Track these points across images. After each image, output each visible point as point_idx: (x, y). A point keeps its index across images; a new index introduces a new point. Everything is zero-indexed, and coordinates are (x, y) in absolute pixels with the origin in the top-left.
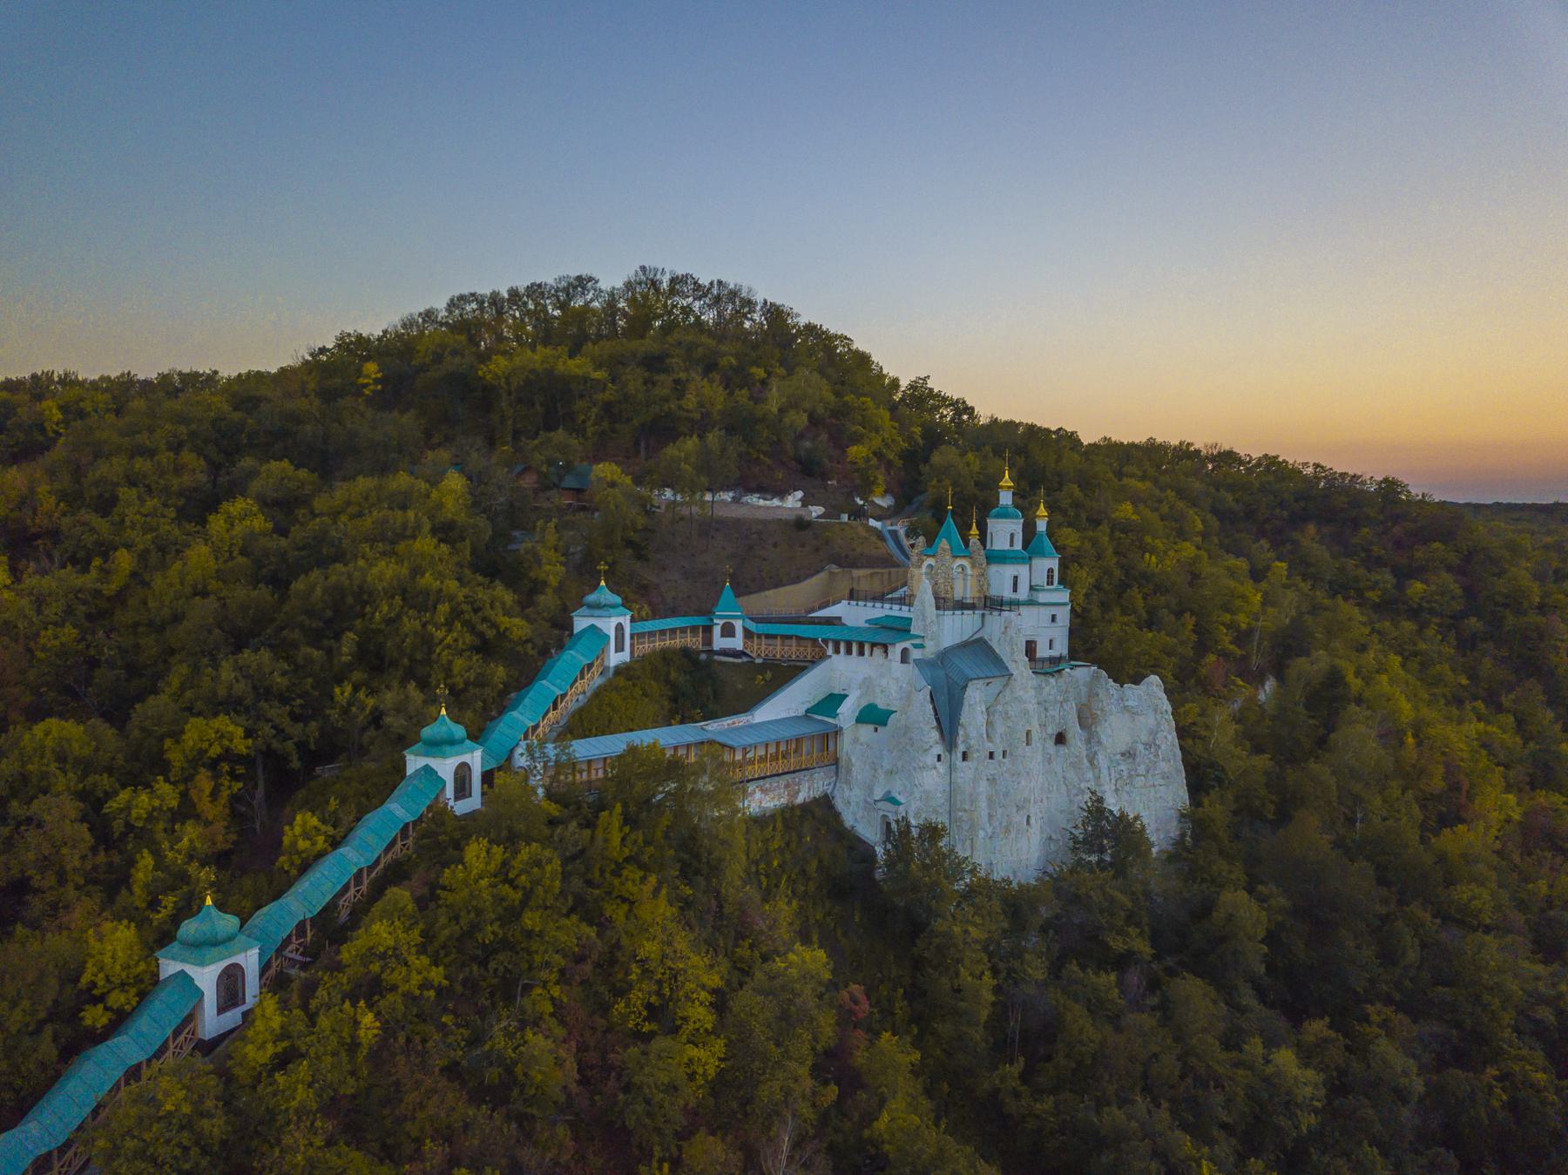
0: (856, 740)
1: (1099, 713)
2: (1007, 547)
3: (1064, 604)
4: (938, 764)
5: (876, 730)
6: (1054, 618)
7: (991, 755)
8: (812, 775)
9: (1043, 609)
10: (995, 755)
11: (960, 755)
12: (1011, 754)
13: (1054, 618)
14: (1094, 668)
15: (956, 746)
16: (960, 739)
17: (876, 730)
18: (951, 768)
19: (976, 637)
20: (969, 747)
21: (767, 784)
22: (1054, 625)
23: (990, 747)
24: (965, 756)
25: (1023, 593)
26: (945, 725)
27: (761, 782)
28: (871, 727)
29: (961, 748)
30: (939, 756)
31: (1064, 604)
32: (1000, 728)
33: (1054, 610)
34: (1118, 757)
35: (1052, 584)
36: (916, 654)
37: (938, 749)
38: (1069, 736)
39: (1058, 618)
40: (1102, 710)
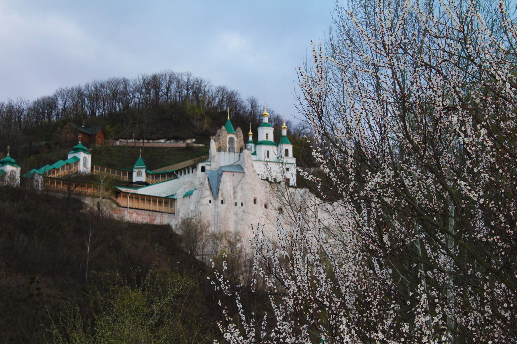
0: (183, 204)
7: (236, 204)
8: (162, 215)
10: (238, 204)
11: (220, 202)
12: (245, 204)
14: (304, 189)
15: (218, 197)
16: (220, 195)
18: (216, 206)
19: (237, 163)
20: (224, 199)
21: (139, 212)
23: (236, 201)
24: (222, 202)
26: (214, 189)
27: (136, 210)
28: (188, 197)
29: (220, 198)
30: (210, 202)
32: (239, 194)
36: (207, 168)
37: (211, 198)
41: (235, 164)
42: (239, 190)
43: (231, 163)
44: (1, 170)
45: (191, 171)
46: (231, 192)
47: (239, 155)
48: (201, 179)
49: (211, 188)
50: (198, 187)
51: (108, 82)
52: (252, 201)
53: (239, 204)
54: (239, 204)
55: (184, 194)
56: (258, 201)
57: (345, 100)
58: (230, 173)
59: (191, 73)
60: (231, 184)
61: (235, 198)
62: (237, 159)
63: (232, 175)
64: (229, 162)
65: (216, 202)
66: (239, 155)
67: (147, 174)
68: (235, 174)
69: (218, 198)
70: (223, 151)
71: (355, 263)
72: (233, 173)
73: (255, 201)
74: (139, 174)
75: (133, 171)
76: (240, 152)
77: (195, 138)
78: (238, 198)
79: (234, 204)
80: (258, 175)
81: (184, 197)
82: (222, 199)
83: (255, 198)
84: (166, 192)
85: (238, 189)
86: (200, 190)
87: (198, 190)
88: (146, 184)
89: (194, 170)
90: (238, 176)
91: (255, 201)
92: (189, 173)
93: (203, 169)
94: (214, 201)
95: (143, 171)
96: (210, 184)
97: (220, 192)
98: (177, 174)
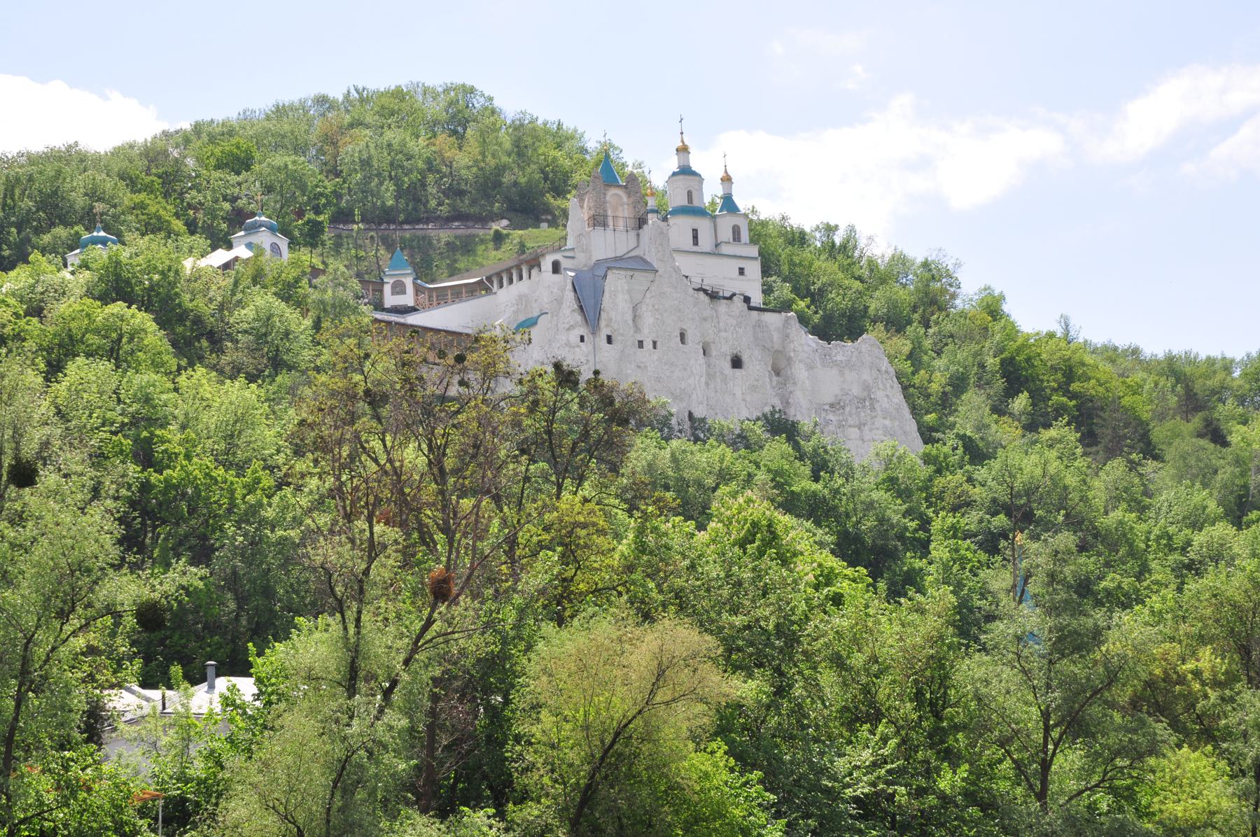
1: (792, 354)
2: (685, 203)
3: (755, 259)
6: (741, 271)
7: (641, 344)
9: (725, 260)
13: (741, 271)
16: (603, 323)
22: (742, 277)
24: (609, 340)
25: (706, 242)
29: (604, 332)
30: (582, 339)
31: (755, 259)
33: (742, 264)
36: (565, 263)
37: (582, 331)
39: (746, 272)
40: (794, 351)
41: (629, 255)
42: (645, 310)
43: (619, 254)
45: (525, 275)
46: (629, 317)
47: (638, 235)
48: (555, 291)
49: (581, 307)
51: (112, 153)
53: (648, 345)
54: (648, 345)
56: (689, 336)
57: (426, 646)
58: (623, 273)
60: (627, 297)
61: (637, 329)
62: (632, 244)
63: (629, 278)
65: (597, 339)
66: (638, 235)
67: (418, 290)
68: (637, 274)
72: (631, 273)
73: (682, 337)
74: (399, 289)
75: (382, 283)
76: (640, 228)
78: (646, 331)
83: (682, 329)
84: (470, 325)
86: (552, 317)
87: (549, 315)
88: (413, 310)
89: (534, 272)
90: (642, 279)
92: (521, 278)
93: (556, 268)
95: (408, 282)
97: (603, 315)
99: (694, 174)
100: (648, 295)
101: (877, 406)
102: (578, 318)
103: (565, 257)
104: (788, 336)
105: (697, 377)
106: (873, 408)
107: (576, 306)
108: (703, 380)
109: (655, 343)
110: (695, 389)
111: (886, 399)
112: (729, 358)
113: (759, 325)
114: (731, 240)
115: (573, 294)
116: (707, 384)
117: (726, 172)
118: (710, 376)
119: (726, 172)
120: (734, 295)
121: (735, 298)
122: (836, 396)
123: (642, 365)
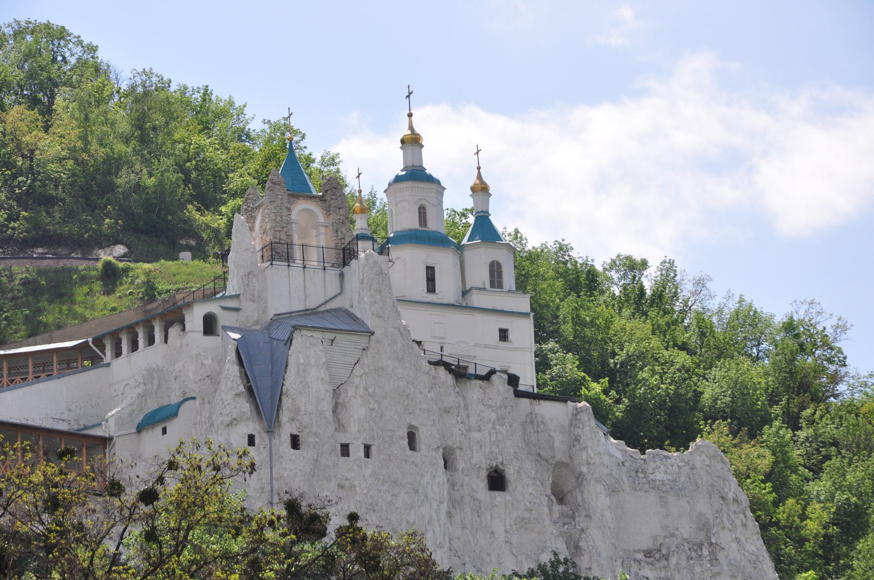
1: (584, 469)
3: (525, 315)
4: (250, 449)
5: (164, 431)
6: (504, 335)
7: (345, 450)
9: (479, 317)
10: (352, 449)
13: (504, 335)
16: (285, 416)
17: (164, 431)
22: (504, 344)
24: (295, 442)
28: (159, 430)
29: (287, 429)
30: (251, 440)
31: (525, 315)
34: (640, 556)
35: (500, 286)
36: (224, 319)
37: (253, 427)
38: (510, 473)
39: (511, 335)
41: (322, 309)
43: (312, 305)
44: (2, 549)
45: (158, 335)
46: (327, 406)
47: (342, 275)
49: (250, 390)
50: (193, 389)
52: (402, 438)
53: (356, 451)
54: (356, 451)
55: (140, 419)
56: (422, 437)
58: (318, 335)
59: (97, 46)
61: (340, 426)
63: (327, 343)
64: (306, 297)
66: (342, 275)
68: (340, 337)
69: (280, 426)
70: (280, 260)
71: (295, 561)
73: (412, 439)
76: (345, 263)
77: (121, 243)
78: (353, 428)
79: (339, 447)
80: (416, 346)
81: (140, 429)
82: (295, 432)
84: (65, 417)
85: (351, 393)
86: (202, 404)
87: (198, 401)
89: (174, 331)
91: (412, 439)
92: (151, 341)
94: (265, 435)
96: (245, 377)
97: (286, 403)
98: (102, 348)
99: (430, 179)
100: (358, 371)
101: (721, 555)
102: (245, 406)
103: (225, 308)
104: (577, 439)
105: (435, 504)
106: (714, 560)
107: (242, 388)
108: (444, 508)
109: (367, 449)
110: (430, 522)
111: (735, 545)
112: (484, 474)
113: (531, 420)
114: (488, 286)
115: (236, 368)
116: (450, 515)
117: (479, 176)
118: (455, 503)
119: (479, 176)
120: (493, 372)
121: (494, 378)
122: (655, 538)
123: (347, 483)
